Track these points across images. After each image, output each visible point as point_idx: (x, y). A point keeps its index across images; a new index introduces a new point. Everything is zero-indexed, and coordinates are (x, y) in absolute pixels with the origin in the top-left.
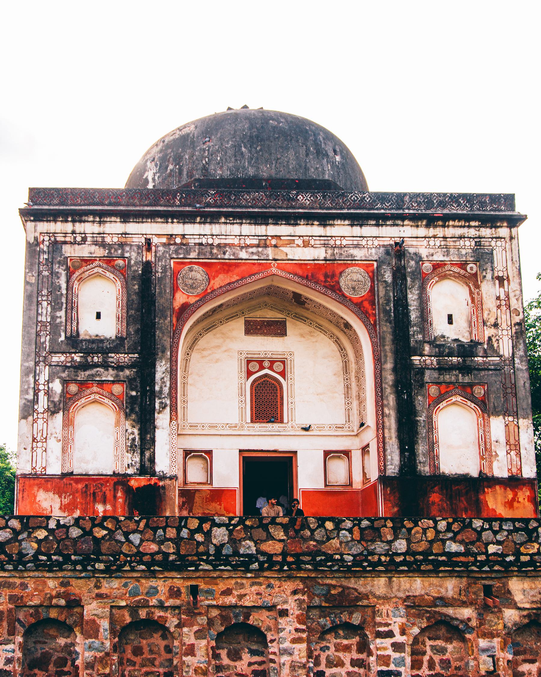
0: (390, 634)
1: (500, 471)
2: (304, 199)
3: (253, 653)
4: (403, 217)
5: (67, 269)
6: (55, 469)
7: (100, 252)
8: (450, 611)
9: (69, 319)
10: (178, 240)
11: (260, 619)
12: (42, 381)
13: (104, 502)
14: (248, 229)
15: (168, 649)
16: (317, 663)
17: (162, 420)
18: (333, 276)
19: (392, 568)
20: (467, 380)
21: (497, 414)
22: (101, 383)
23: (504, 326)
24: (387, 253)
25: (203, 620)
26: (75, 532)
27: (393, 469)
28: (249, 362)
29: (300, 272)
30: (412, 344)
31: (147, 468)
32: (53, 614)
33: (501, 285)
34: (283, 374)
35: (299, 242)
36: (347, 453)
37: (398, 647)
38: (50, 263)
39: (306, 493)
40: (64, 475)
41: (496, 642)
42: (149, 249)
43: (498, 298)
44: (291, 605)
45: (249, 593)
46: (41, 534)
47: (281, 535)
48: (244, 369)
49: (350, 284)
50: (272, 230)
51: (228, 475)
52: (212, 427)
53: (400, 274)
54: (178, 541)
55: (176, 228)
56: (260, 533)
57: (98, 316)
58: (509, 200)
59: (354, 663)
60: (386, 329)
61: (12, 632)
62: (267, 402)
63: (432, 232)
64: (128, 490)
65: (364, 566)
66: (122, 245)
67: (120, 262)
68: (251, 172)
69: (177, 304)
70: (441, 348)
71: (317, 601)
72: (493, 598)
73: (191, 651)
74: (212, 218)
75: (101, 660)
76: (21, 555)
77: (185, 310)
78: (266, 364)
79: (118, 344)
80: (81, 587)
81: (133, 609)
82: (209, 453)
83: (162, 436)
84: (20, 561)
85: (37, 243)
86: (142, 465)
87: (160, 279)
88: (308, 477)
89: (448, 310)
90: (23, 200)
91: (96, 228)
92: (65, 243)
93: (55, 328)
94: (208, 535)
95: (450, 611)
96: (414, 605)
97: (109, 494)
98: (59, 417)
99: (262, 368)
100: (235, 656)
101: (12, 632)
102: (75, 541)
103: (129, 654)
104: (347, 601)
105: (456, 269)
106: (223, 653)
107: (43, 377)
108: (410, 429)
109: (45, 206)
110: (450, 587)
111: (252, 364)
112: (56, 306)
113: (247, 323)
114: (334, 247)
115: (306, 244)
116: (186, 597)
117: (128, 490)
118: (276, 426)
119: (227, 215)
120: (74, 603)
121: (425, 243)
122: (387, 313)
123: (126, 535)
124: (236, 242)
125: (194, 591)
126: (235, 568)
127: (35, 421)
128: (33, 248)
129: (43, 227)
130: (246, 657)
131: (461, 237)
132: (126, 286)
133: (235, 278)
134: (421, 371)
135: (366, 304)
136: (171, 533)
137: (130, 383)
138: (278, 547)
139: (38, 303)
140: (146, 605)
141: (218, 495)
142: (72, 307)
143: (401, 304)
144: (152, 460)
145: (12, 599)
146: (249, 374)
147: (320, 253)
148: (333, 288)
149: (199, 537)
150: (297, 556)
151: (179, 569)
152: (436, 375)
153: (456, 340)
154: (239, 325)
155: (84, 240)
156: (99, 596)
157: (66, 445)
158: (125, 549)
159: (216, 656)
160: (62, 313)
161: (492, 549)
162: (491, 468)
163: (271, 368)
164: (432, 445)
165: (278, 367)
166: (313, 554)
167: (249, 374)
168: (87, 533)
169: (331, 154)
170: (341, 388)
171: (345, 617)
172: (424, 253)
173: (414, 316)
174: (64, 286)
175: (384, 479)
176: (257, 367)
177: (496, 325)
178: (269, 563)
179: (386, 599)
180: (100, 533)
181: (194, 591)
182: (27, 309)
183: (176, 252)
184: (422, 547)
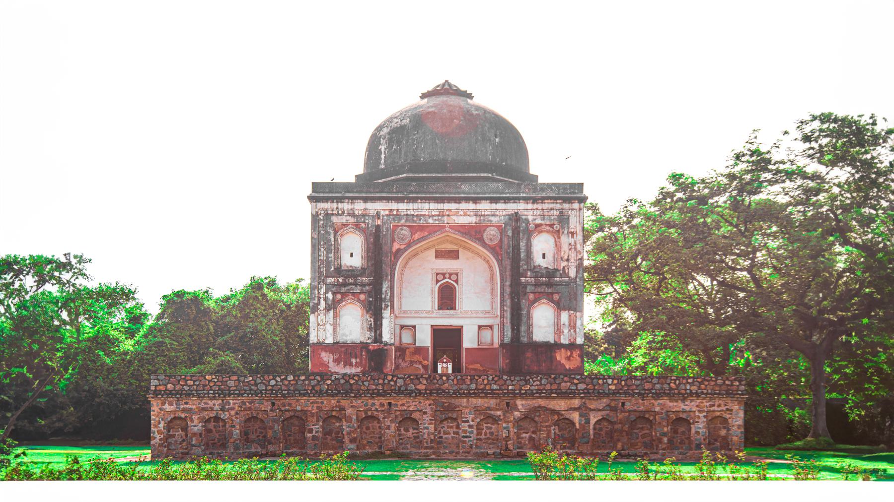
0: (468, 422)
1: (564, 340)
2: (465, 187)
3: (414, 429)
4: (519, 199)
5: (334, 230)
6: (330, 340)
7: (352, 220)
8: (492, 412)
9: (336, 258)
10: (395, 213)
11: (415, 415)
12: (322, 293)
13: (356, 358)
14: (433, 206)
15: (380, 428)
16: (439, 433)
17: (386, 314)
18: (480, 232)
19: (469, 395)
20: (550, 291)
21: (565, 310)
22: (353, 294)
23: (572, 260)
24: (510, 219)
25: (393, 416)
26: (342, 381)
27: (507, 340)
28: (437, 274)
29: (460, 229)
30: (521, 271)
31: (378, 339)
32: (334, 414)
33: (573, 237)
34: (456, 281)
35: (461, 213)
36: (491, 327)
37: (470, 426)
38: (325, 226)
39: (467, 350)
40: (334, 343)
41: (510, 425)
42: (379, 218)
43: (570, 244)
44: (428, 410)
45: (411, 405)
46: (329, 382)
47: (425, 382)
48: (435, 279)
49: (490, 237)
50: (447, 206)
51: (425, 339)
52: (416, 312)
53: (516, 231)
54: (383, 385)
55: (394, 206)
56: (416, 381)
57: (352, 255)
58: (580, 186)
59: (454, 433)
60: (507, 263)
61: (318, 421)
62: (447, 298)
63: (535, 206)
64: (368, 351)
65: (458, 394)
66: (364, 215)
67: (363, 225)
68: (442, 156)
69: (394, 249)
70: (537, 272)
71: (438, 408)
72: (510, 407)
73: (388, 428)
74: (414, 200)
75: (353, 432)
76: (321, 390)
77: (399, 253)
78: (447, 276)
79: (362, 272)
80: (344, 403)
81: (366, 412)
82: (414, 327)
83: (386, 323)
84: (320, 393)
85: (317, 214)
86: (375, 338)
87: (385, 235)
88: (469, 341)
89: (542, 248)
90: (309, 191)
91: (350, 206)
92: (333, 214)
93: (328, 263)
94: (395, 382)
95: (492, 412)
96: (477, 410)
97: (358, 354)
98: (332, 312)
99: (445, 278)
100: (407, 430)
101: (318, 421)
102: (342, 385)
103: (364, 430)
104: (451, 408)
105: (548, 228)
106: (402, 429)
107: (323, 291)
108: (518, 317)
109: (322, 192)
110: (492, 402)
111: (439, 276)
112: (328, 251)
113: (437, 251)
114: (480, 216)
115: (465, 215)
116: (386, 406)
117: (368, 351)
118: (452, 312)
119: (422, 198)
120: (343, 409)
121: (531, 212)
122: (508, 253)
123: (363, 382)
124: (427, 213)
125: (390, 404)
126: (405, 395)
127: (319, 315)
128: (315, 218)
129: (321, 205)
130: (411, 431)
131: (552, 209)
132: (366, 239)
133: (426, 233)
134: (525, 286)
135: (497, 248)
136: (381, 381)
137: (369, 293)
138: (424, 387)
139: (319, 250)
140: (371, 410)
141: (420, 351)
142: (337, 251)
143: (516, 248)
144: (381, 335)
145: (318, 408)
146: (437, 281)
147: (473, 220)
148: (481, 240)
149: (392, 383)
150: (431, 390)
151: (383, 396)
152: (533, 288)
153: (547, 268)
154: (432, 253)
155: (343, 212)
156: (352, 407)
157: (336, 327)
158: (362, 388)
159: (398, 430)
160: (332, 255)
161: (510, 388)
162: (560, 339)
163: (450, 278)
164: (529, 326)
165: (454, 277)
166: (437, 390)
167: (437, 281)
168: (347, 382)
169: (492, 138)
170: (489, 289)
171: (450, 415)
172: (530, 218)
173: (523, 255)
174: (333, 239)
175: (502, 345)
176: (442, 277)
177: (568, 260)
178: (419, 393)
179: (466, 407)
180: (352, 382)
181: (390, 404)
182: (313, 253)
183: (394, 219)
184: (482, 387)
